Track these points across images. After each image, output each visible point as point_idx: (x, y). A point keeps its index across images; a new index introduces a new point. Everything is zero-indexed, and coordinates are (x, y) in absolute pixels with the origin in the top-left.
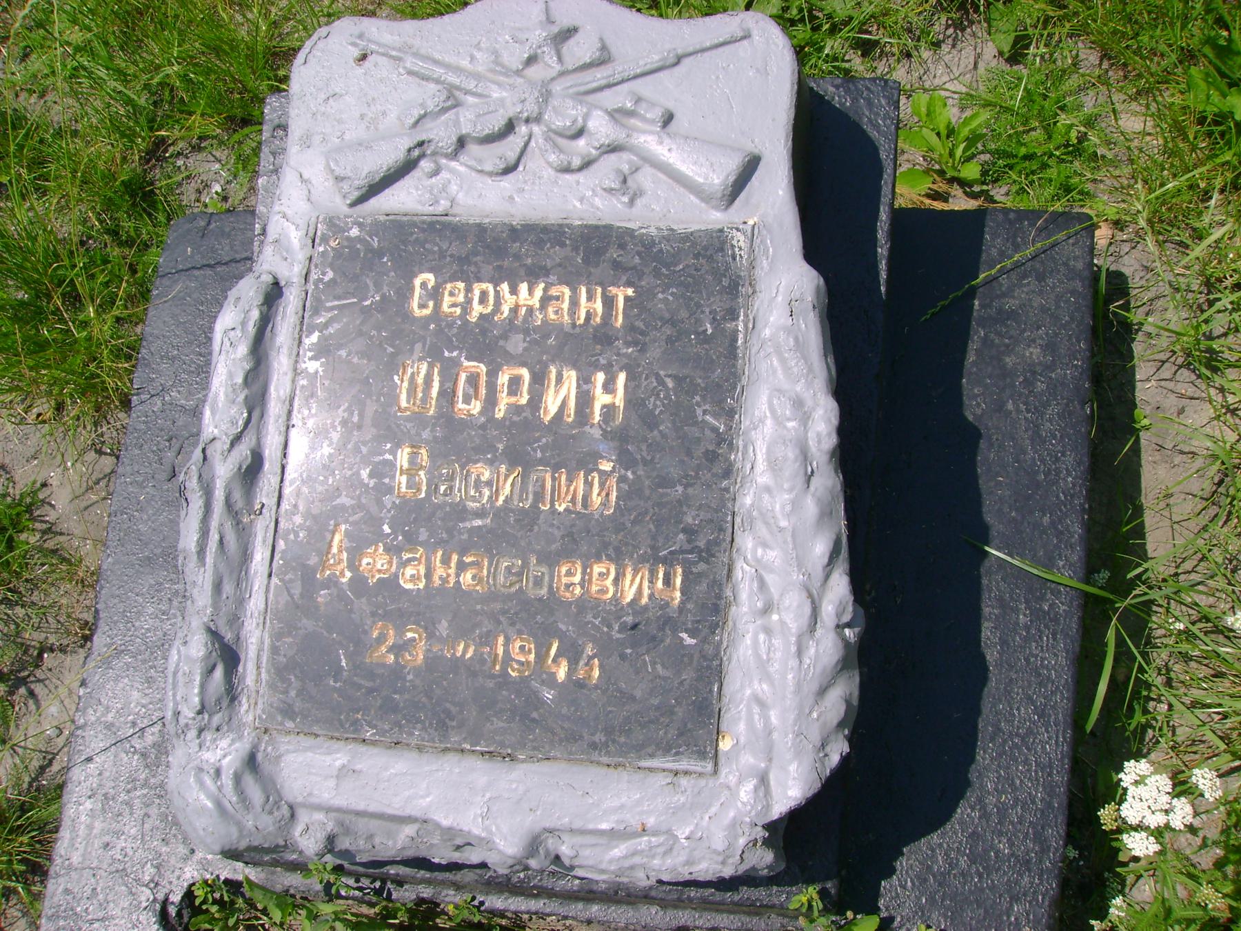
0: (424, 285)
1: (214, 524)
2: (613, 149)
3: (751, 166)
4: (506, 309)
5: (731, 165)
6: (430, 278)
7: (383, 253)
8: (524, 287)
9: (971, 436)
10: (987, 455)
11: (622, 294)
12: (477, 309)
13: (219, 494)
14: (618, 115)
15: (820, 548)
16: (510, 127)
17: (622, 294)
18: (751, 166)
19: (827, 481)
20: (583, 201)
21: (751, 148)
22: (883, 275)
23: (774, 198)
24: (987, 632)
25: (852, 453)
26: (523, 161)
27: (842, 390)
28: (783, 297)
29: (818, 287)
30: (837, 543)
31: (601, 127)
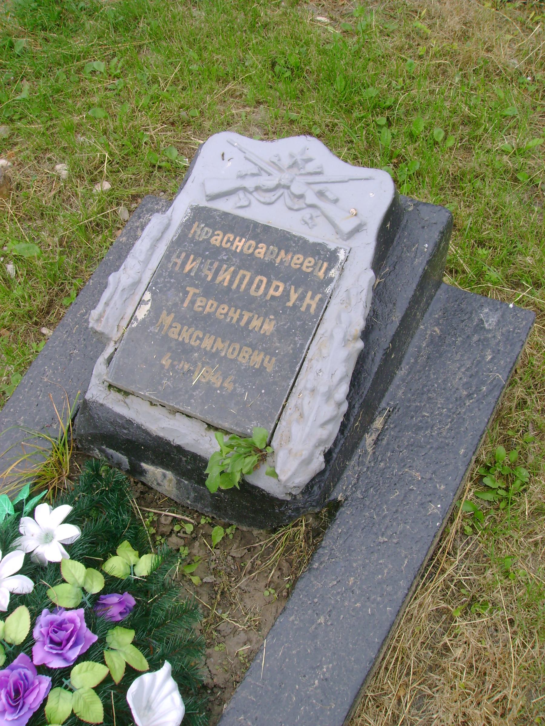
3: (357, 229)
18: (357, 229)
23: (365, 247)
31: (311, 198)
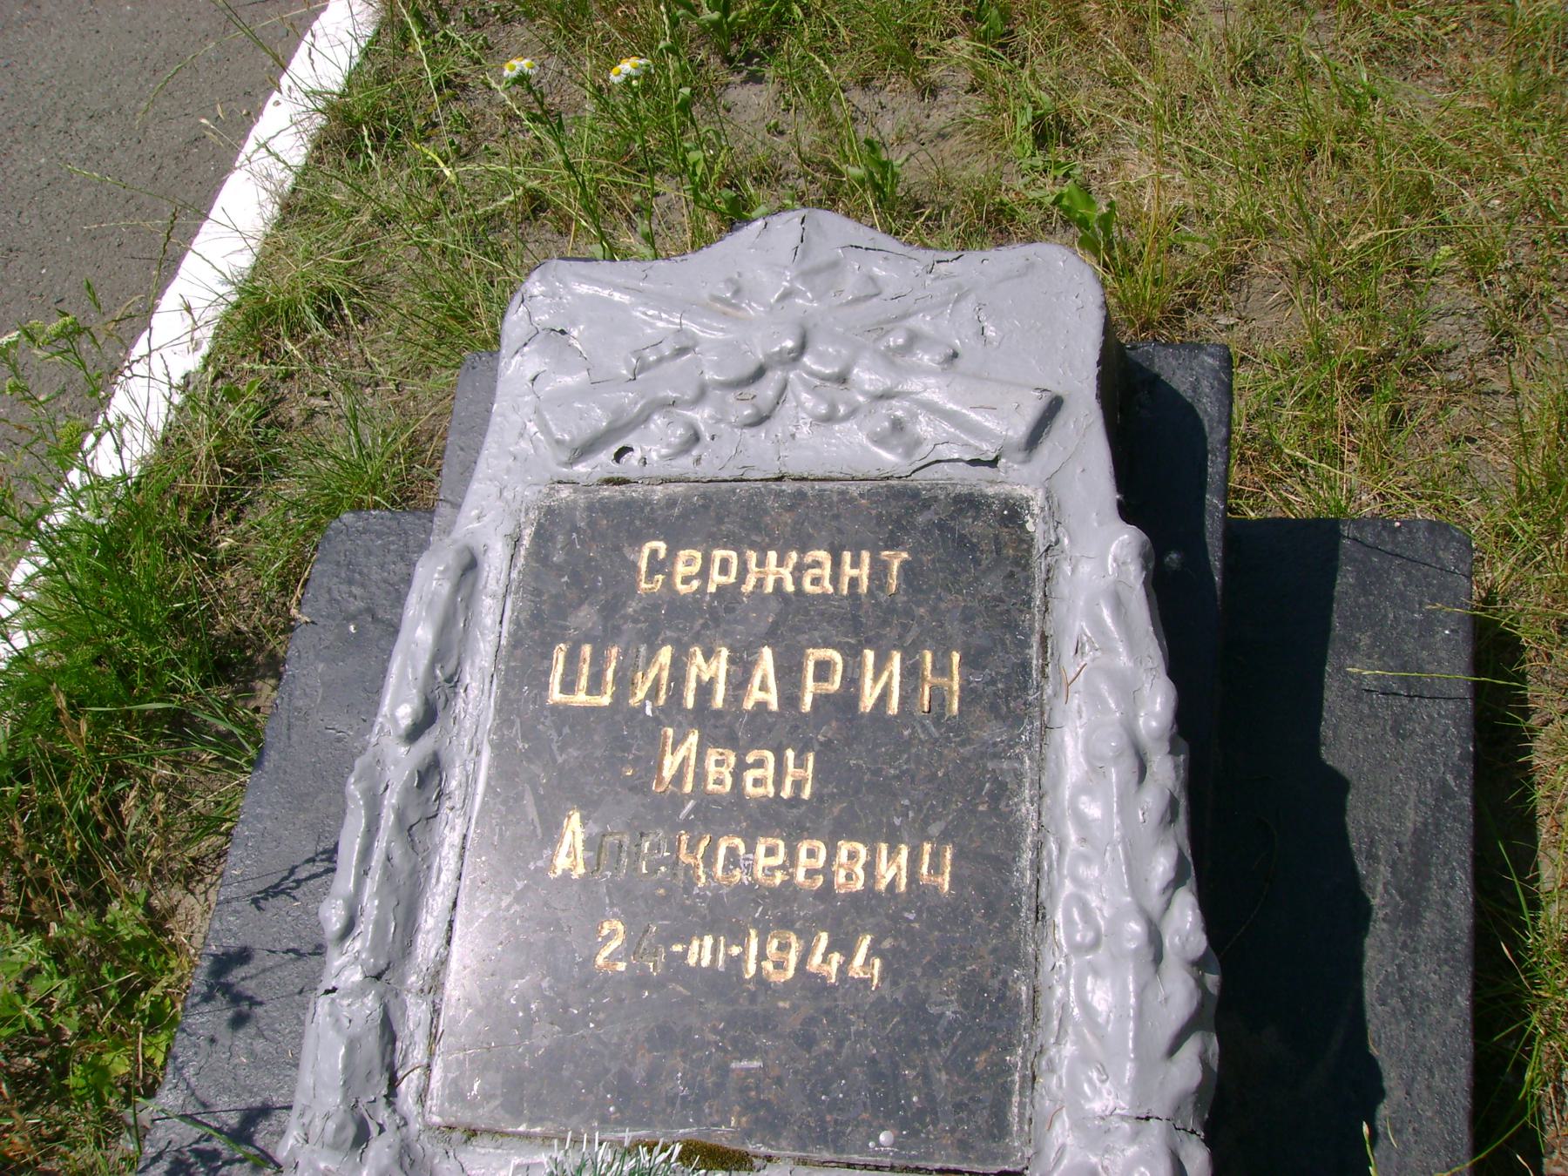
0: (654, 553)
1: (380, 846)
2: (885, 396)
3: (1054, 407)
4: (751, 581)
5: (1032, 408)
6: (661, 546)
7: (585, 559)
8: (772, 556)
9: (1338, 785)
10: (1359, 816)
11: (896, 559)
12: (716, 579)
13: (391, 800)
14: (892, 358)
15: (1162, 866)
16: (760, 373)
17: (896, 559)
18: (1054, 407)
19: (1165, 771)
20: (854, 450)
21: (1059, 390)
22: (1216, 565)
23: (1084, 459)
24: (1378, 1015)
25: (1191, 726)
26: (506, 1139)
27: (1178, 668)
28: (1097, 566)
29: (1143, 546)
30: (1181, 858)
